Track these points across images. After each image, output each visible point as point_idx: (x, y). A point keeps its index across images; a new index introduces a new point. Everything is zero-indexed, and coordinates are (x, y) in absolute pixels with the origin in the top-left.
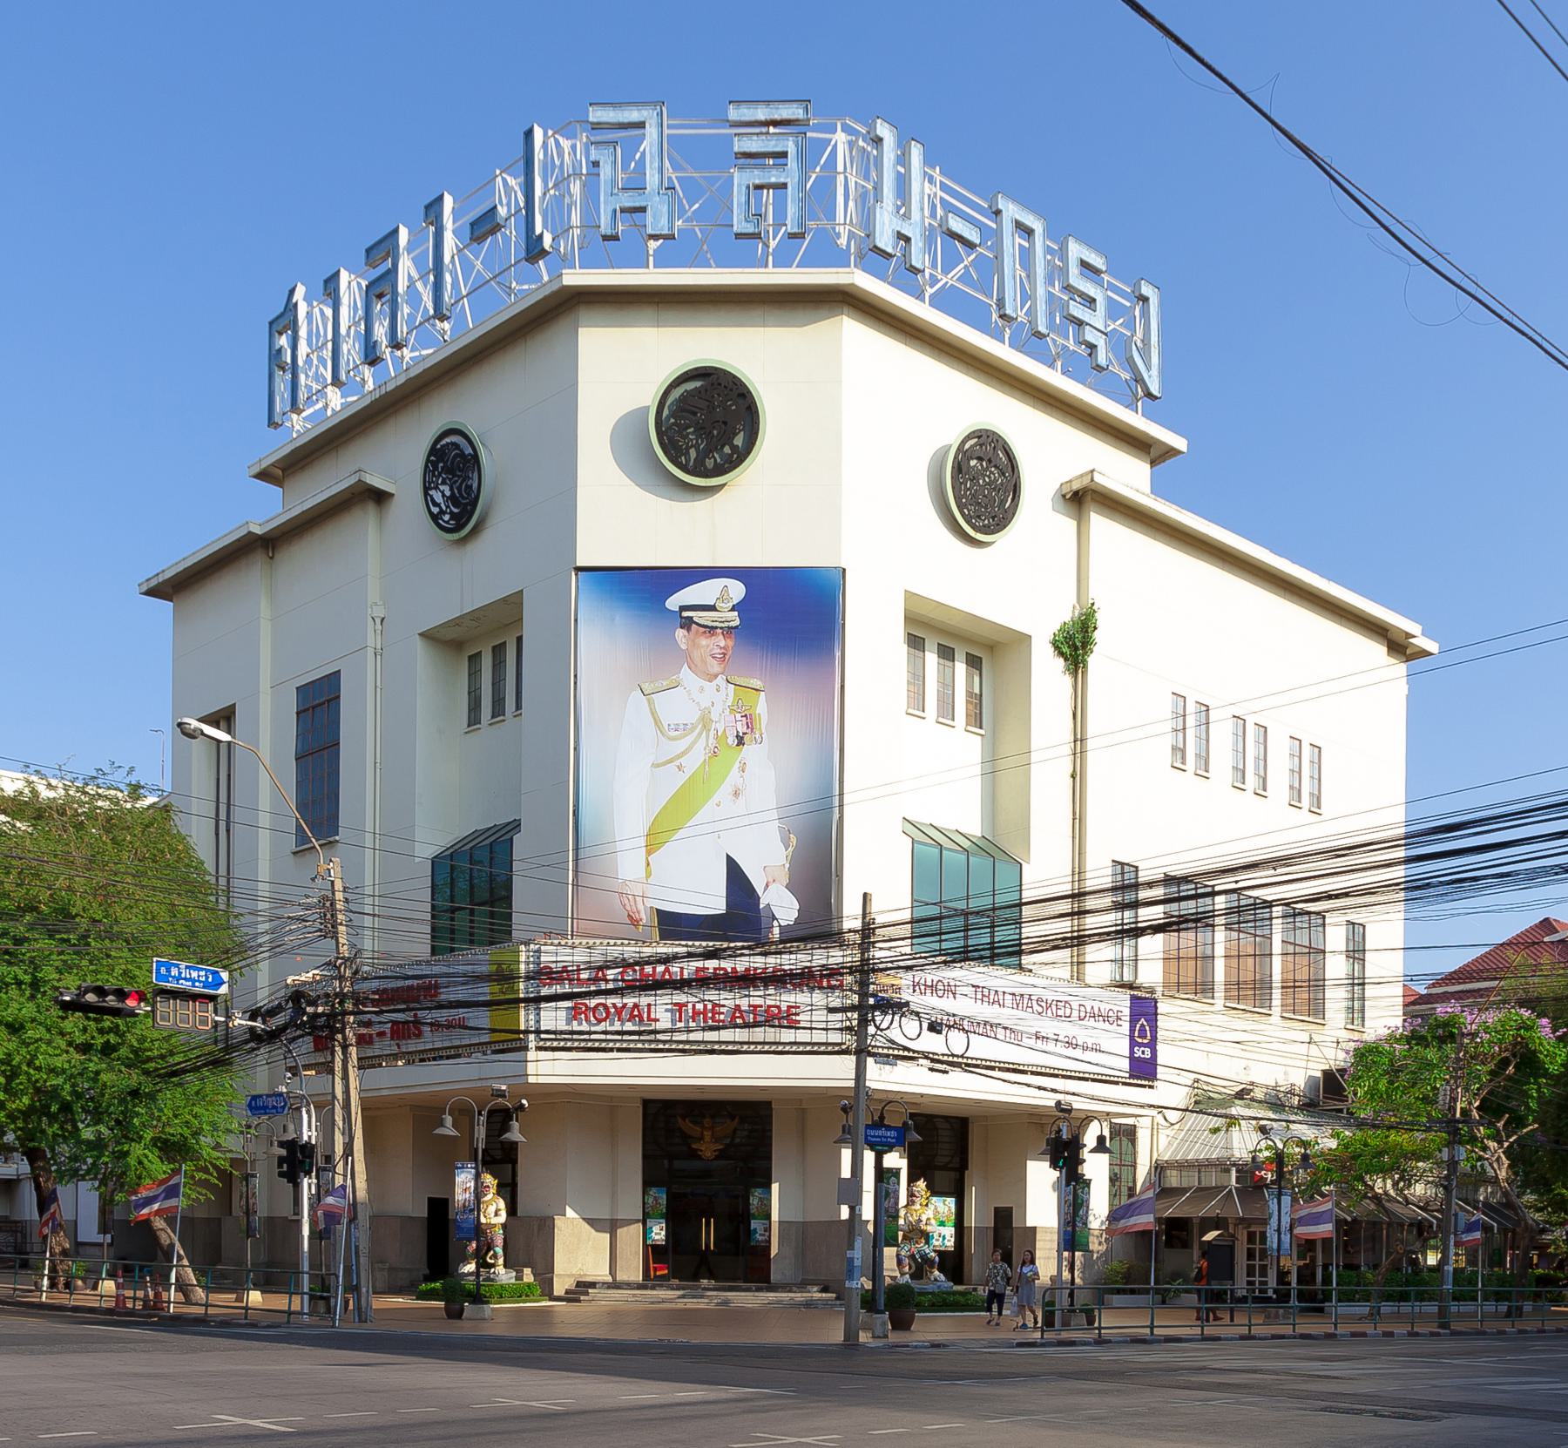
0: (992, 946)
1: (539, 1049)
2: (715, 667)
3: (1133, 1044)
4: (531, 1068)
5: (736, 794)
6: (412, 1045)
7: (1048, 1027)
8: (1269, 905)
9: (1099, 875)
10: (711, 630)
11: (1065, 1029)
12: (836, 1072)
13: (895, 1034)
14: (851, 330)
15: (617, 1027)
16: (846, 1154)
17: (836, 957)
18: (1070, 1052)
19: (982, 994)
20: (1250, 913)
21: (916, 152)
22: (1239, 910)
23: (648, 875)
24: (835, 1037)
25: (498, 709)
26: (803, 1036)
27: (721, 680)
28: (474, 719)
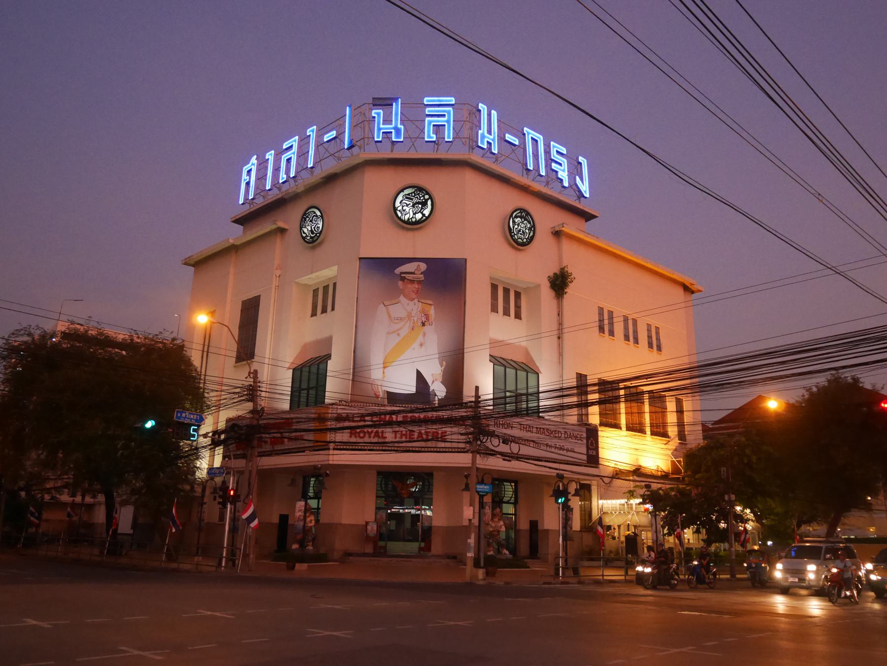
0: (527, 409)
1: (334, 449)
2: (414, 296)
3: (588, 449)
4: (101, 521)
5: (421, 345)
6: (278, 447)
7: (552, 442)
8: (643, 393)
9: (571, 380)
10: (412, 282)
11: (559, 443)
12: (463, 460)
13: (488, 444)
14: (469, 176)
15: (367, 439)
16: (452, 100)
17: (462, 413)
18: (561, 452)
19: (523, 427)
20: (634, 397)
21: (494, 113)
22: (631, 395)
23: (384, 377)
24: (463, 445)
25: (324, 311)
26: (448, 445)
27: (416, 301)
28: (314, 314)
